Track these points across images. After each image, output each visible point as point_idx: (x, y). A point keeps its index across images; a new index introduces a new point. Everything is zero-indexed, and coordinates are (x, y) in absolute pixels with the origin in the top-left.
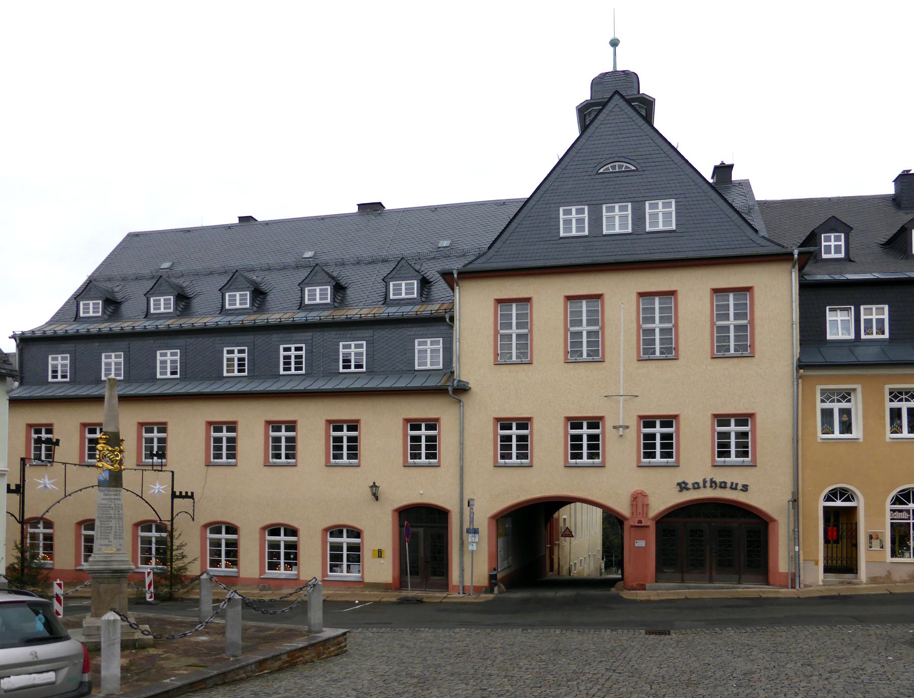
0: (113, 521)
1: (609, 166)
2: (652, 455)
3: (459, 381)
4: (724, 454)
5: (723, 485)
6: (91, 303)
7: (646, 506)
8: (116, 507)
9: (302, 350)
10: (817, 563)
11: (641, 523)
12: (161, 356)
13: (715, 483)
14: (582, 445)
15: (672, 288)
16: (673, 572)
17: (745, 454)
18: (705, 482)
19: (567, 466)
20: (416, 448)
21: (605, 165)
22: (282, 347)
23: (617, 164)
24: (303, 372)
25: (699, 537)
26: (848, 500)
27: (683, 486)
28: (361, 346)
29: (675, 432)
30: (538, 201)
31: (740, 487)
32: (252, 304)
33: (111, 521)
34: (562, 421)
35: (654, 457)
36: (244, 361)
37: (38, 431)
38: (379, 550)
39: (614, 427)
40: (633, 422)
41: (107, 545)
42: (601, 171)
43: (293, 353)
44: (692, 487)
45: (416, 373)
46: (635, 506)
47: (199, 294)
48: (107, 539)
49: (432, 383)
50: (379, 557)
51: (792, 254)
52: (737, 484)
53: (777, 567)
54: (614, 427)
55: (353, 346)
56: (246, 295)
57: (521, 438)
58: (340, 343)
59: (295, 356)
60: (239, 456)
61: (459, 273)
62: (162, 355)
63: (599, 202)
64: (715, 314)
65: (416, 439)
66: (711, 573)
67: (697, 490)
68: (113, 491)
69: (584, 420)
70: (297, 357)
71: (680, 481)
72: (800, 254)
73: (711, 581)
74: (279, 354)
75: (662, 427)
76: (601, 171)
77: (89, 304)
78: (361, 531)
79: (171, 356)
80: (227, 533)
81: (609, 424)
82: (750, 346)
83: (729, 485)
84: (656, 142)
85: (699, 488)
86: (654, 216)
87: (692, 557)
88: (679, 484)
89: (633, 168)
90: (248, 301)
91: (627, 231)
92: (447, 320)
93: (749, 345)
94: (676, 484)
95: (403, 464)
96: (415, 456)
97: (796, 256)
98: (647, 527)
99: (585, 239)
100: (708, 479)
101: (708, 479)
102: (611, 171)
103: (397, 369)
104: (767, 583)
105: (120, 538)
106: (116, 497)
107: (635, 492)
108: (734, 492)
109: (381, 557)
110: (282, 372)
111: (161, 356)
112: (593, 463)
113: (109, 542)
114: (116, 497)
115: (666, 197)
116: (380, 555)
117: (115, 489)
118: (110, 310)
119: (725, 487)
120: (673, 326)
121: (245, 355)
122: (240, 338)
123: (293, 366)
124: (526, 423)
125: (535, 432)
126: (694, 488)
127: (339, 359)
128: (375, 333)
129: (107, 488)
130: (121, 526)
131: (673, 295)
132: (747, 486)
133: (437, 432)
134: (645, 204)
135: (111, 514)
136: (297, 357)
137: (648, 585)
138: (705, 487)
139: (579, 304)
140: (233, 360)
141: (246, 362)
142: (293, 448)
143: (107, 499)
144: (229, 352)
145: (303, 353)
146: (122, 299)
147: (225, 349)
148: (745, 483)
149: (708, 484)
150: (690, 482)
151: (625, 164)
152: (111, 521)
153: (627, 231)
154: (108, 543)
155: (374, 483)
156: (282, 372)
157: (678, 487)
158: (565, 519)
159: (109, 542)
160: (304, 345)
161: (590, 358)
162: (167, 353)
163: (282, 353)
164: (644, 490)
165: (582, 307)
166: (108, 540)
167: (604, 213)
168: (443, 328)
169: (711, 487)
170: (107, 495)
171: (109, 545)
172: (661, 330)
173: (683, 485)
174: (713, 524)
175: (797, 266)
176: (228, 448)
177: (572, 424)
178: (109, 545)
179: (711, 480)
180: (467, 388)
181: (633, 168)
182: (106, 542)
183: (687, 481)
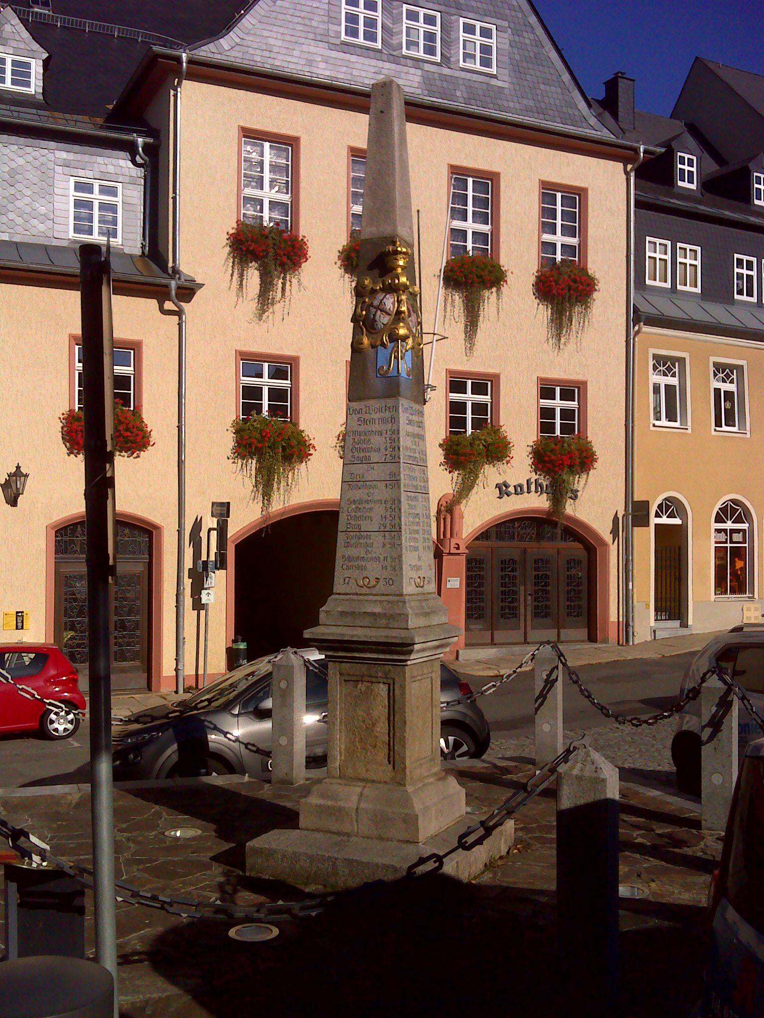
26: (738, 520)
38: (17, 613)
44: (513, 492)
50: (17, 628)
64: (451, 193)
85: (522, 493)
87: (503, 604)
88: (498, 486)
109: (22, 628)
116: (20, 625)
121: (736, 270)
124: (574, 397)
126: (516, 493)
149: (533, 487)
150: (512, 482)
155: (18, 467)
170: (365, 422)
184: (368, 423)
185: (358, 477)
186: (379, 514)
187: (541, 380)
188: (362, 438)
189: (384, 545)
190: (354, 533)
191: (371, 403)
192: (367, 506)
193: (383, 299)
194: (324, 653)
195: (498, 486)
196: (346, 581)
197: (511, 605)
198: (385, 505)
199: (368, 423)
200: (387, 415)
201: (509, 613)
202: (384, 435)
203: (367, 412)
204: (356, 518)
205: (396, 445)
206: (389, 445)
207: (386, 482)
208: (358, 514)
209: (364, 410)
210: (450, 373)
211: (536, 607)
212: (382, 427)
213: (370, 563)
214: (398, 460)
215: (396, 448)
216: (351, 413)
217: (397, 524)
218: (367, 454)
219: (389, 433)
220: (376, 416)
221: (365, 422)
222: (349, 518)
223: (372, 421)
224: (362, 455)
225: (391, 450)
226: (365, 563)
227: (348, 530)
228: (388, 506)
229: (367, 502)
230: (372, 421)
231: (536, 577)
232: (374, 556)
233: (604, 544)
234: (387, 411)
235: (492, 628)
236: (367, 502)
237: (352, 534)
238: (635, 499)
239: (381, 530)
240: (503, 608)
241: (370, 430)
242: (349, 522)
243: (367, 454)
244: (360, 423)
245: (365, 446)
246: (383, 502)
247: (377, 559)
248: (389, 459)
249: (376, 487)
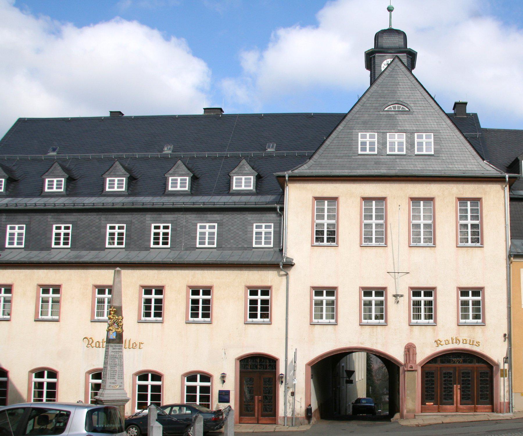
0: (118, 366)
1: (391, 106)
2: (418, 317)
3: (287, 258)
4: (148, 315)
6: (116, 179)
7: (415, 354)
8: (119, 357)
9: (123, 229)
11: (412, 368)
12: (256, 228)
19: (246, 324)
20: (148, 308)
21: (389, 106)
22: (54, 226)
23: (397, 105)
24: (169, 246)
25: (450, 378)
28: (270, 227)
29: (482, 300)
30: (345, 127)
32: (6, 189)
33: (116, 367)
34: (138, 288)
35: (256, 317)
36: (168, 235)
37: (46, 291)
39: (394, 296)
41: (114, 383)
42: (386, 109)
43: (161, 231)
45: (254, 250)
47: (83, 176)
48: (114, 379)
49: (267, 259)
51: (505, 178)
55: (264, 227)
56: (123, 180)
58: (254, 224)
59: (18, 233)
60: (13, 314)
61: (289, 177)
62: (201, 227)
65: (369, 304)
68: (118, 346)
70: (164, 234)
72: (509, 178)
74: (151, 231)
75: (425, 296)
76: (386, 109)
77: (114, 181)
78: (162, 376)
79: (265, 228)
80: (153, 380)
81: (391, 292)
84: (421, 93)
86: (420, 144)
89: (407, 109)
90: (63, 186)
91: (431, 153)
92: (278, 210)
95: (244, 322)
96: (148, 315)
97: (507, 179)
98: (416, 371)
99: (375, 157)
102: (393, 109)
103: (240, 246)
105: (121, 378)
106: (120, 350)
110: (152, 246)
111: (256, 228)
112: (252, 321)
113: (115, 381)
114: (120, 350)
117: (119, 345)
118: (11, 188)
121: (124, 231)
122: (119, 217)
123: (62, 241)
125: (166, 297)
127: (253, 237)
128: (225, 217)
129: (115, 344)
130: (122, 370)
131: (432, 200)
133: (335, 297)
134: (414, 135)
135: (116, 362)
136: (164, 234)
139: (370, 203)
140: (260, 233)
141: (124, 237)
143: (114, 352)
144: (12, 228)
145: (70, 231)
146: (19, 177)
147: (108, 226)
149: (454, 341)
151: (402, 106)
152: (116, 367)
153: (431, 153)
154: (114, 382)
156: (152, 246)
158: (343, 366)
159: (115, 381)
160: (125, 225)
161: (426, 244)
162: (262, 226)
163: (55, 231)
165: (372, 206)
166: (115, 380)
167: (388, 139)
168: (273, 216)
170: (114, 349)
171: (115, 383)
172: (377, 225)
173: (439, 342)
175: (508, 186)
176: (262, 309)
177: (413, 292)
178: (115, 383)
180: (293, 264)
181: (407, 109)
182: (113, 381)
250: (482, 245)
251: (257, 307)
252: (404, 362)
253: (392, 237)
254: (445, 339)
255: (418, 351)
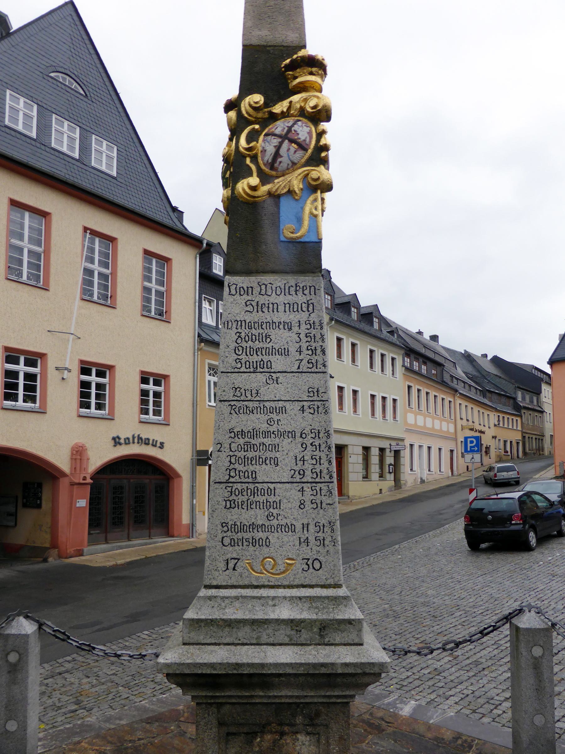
5: (147, 442)
10: (204, 514)
13: (141, 439)
14: (17, 384)
15: (114, 235)
16: (98, 533)
17: (33, 399)
18: (134, 437)
27: (116, 441)
31: (158, 445)
39: (57, 369)
40: (76, 368)
42: (52, 75)
46: (78, 461)
52: (156, 441)
53: (180, 519)
54: (57, 369)
57: (30, 377)
63: (92, 131)
66: (129, 530)
67: (128, 446)
69: (22, 355)
71: (115, 436)
73: (129, 539)
76: (52, 75)
81: (52, 363)
82: (166, 313)
83: (151, 442)
88: (114, 439)
93: (109, 296)
94: (111, 438)
97: (205, 245)
99: (74, 162)
100: (136, 435)
101: (136, 435)
104: (169, 534)
107: (76, 444)
108: (154, 448)
115: (15, 90)
119: (148, 444)
120: (111, 274)
126: (126, 444)
132: (163, 443)
137: (86, 550)
138: (134, 443)
142: (8, 386)
148: (162, 441)
149: (136, 440)
150: (123, 437)
157: (113, 442)
164: (87, 445)
169: (138, 443)
170: (260, 307)
173: (117, 440)
174: (132, 480)
179: (139, 436)
183: (120, 436)
184: (265, 310)
185: (248, 394)
186: (291, 454)
187: (142, 372)
188: (254, 331)
189: (302, 505)
190: (245, 486)
191: (267, 279)
192: (267, 441)
193: (292, 126)
194: (189, 694)
195: (114, 439)
196: (231, 565)
197: (120, 516)
198: (301, 440)
199: (265, 310)
200: (300, 299)
201: (118, 522)
202: (295, 329)
203: (263, 292)
204: (246, 460)
205: (318, 345)
206: (304, 346)
207: (301, 404)
208: (250, 454)
209: (256, 290)
210: (82, 362)
211: (136, 517)
212: (293, 317)
213: (276, 534)
214: (323, 369)
215: (319, 351)
216: (233, 292)
217: (325, 471)
218: (266, 358)
219: (303, 326)
220: (281, 299)
221: (260, 307)
222: (233, 460)
223: (275, 307)
224: (255, 358)
225: (310, 352)
226: (266, 534)
227: (232, 480)
228: (309, 441)
229: (267, 434)
230: (275, 307)
231: (136, 497)
232: (283, 522)
233: (178, 476)
234: (300, 293)
235: (106, 532)
236: (267, 434)
237: (239, 486)
238: (198, 449)
239: (295, 480)
240: (113, 519)
241: (269, 319)
242: (232, 466)
243: (266, 358)
244: (250, 308)
245: (261, 345)
246: (298, 435)
247: (291, 528)
248: (304, 366)
249: (283, 410)
250: (148, 303)
251: (25, 390)
252: (71, 471)
253: (279, 372)
254: (126, 437)
255: (91, 454)
